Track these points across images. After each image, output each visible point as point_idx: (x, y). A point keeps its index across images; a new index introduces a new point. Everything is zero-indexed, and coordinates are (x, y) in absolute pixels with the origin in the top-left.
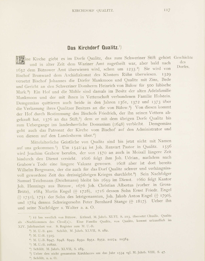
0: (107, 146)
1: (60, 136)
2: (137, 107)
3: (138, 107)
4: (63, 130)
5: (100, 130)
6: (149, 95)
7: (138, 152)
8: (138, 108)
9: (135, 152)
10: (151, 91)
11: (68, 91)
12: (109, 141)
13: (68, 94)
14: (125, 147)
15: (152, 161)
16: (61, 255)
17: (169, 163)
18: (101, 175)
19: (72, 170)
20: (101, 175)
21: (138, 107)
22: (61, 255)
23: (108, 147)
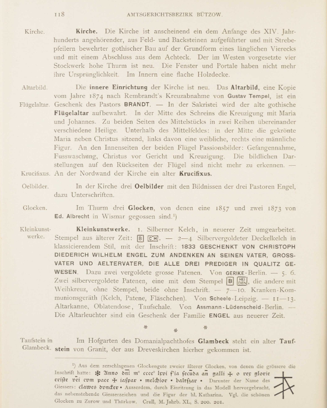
0: (127, 94)
1: (237, 299)
2: (197, 297)
3: (199, 298)
4: (274, 255)
5: (181, 350)
6: (200, 314)
7: (291, 86)
8: (198, 299)
9: (202, 281)
10: (170, 58)
11: (190, 105)
12: (58, 348)
13: (190, 108)
14: (129, 298)
15: (190, 277)
16: (209, 352)
17: (246, 140)
18: (171, 97)
19: (157, 49)
20: (171, 97)
21: (199, 298)
22: (209, 352)
23: (129, 96)
